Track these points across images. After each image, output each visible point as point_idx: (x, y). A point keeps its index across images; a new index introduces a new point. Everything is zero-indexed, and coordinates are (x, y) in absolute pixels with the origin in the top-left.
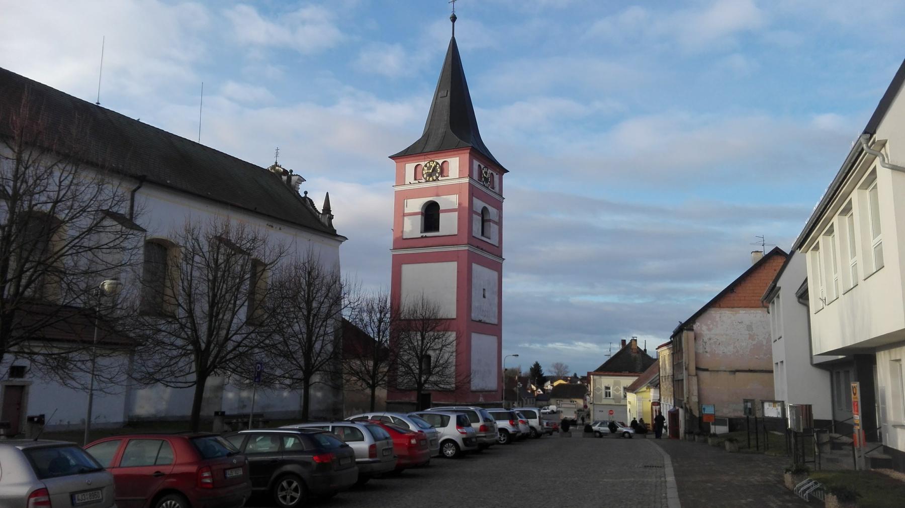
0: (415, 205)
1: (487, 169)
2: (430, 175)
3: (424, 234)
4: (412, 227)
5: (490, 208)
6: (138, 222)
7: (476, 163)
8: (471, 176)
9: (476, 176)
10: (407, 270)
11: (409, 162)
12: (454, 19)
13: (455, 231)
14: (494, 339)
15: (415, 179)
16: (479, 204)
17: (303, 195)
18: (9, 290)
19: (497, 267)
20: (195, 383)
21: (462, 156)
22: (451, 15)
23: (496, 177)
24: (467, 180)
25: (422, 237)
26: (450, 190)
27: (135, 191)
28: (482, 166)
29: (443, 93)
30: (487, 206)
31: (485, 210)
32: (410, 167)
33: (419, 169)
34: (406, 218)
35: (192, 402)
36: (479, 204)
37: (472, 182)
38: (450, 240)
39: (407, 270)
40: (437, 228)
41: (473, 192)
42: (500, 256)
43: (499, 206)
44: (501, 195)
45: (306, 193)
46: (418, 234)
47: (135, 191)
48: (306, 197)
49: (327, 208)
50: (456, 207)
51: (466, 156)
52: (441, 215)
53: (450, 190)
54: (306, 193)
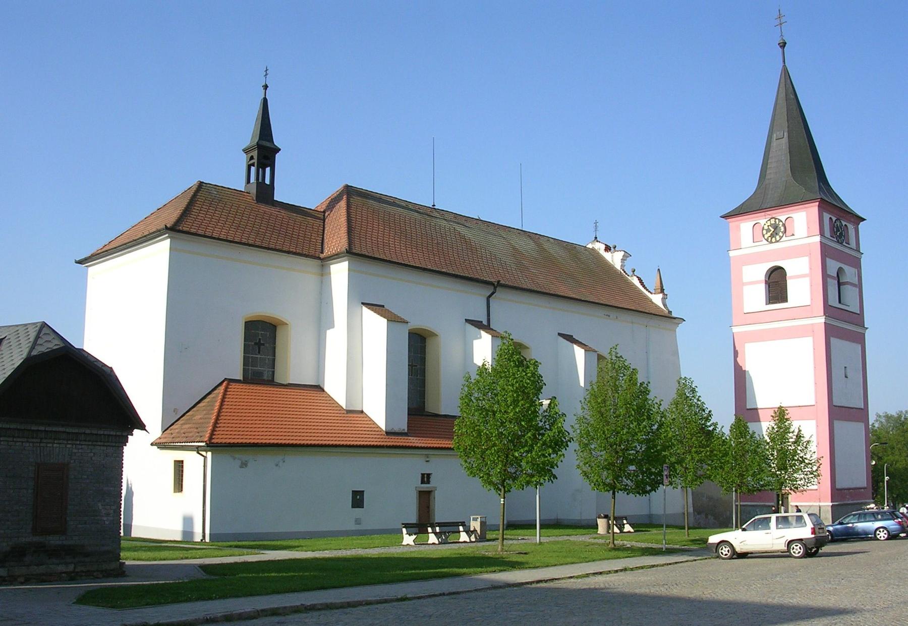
1: (840, 222)
5: (846, 268)
6: (674, 315)
7: (827, 216)
8: (822, 234)
9: (827, 233)
12: (783, 45)
13: (807, 302)
14: (836, 402)
16: (833, 266)
18: (164, 495)
19: (860, 339)
20: (744, 284)
23: (851, 227)
24: (817, 239)
27: (490, 296)
28: (834, 219)
30: (843, 266)
31: (840, 271)
36: (833, 266)
37: (825, 241)
40: (784, 299)
41: (826, 252)
42: (862, 324)
43: (856, 263)
44: (858, 250)
47: (490, 296)
51: (813, 209)
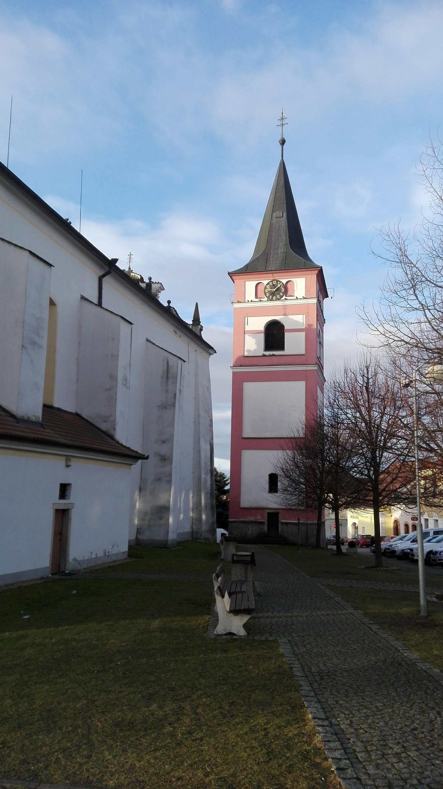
0: (258, 324)
2: (273, 294)
3: (267, 353)
4: (254, 345)
10: (249, 387)
11: (249, 280)
15: (256, 296)
17: (166, 305)
21: (309, 276)
22: (279, 138)
25: (264, 356)
26: (297, 310)
29: (278, 213)
32: (250, 285)
33: (259, 287)
34: (247, 336)
35: (326, 532)
38: (295, 359)
39: (249, 387)
45: (169, 302)
46: (261, 352)
47: (103, 276)
48: (169, 307)
49: (196, 320)
50: (304, 327)
52: (287, 335)
53: (297, 310)
54: (169, 302)
